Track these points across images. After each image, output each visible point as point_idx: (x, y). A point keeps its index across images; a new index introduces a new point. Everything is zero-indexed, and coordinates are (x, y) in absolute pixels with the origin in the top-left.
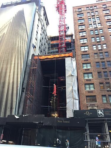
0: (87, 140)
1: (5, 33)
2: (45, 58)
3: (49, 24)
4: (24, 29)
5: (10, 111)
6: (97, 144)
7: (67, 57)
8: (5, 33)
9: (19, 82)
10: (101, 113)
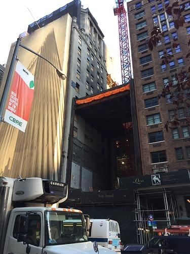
0: (138, 220)
2: (91, 101)
3: (103, 36)
9: (56, 144)
10: (157, 179)
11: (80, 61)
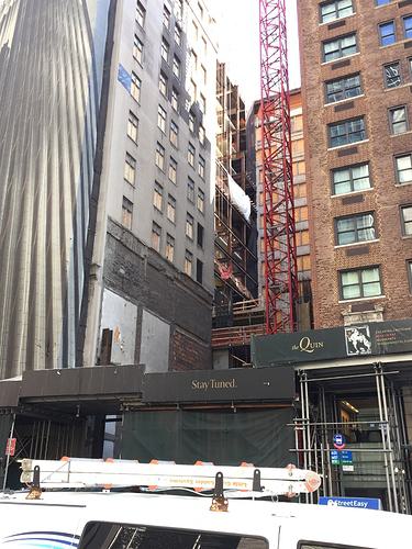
0: (301, 446)
1: (9, 46)
4: (76, 10)
5: (44, 356)
8: (9, 46)
10: (362, 338)
11: (144, 10)
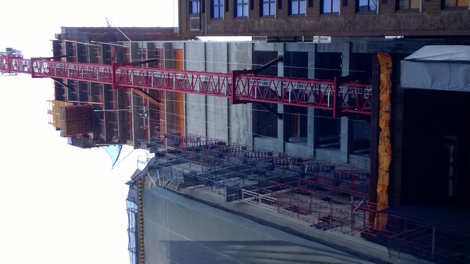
3: (55, 42)
6: (316, 39)
7: (312, 80)
